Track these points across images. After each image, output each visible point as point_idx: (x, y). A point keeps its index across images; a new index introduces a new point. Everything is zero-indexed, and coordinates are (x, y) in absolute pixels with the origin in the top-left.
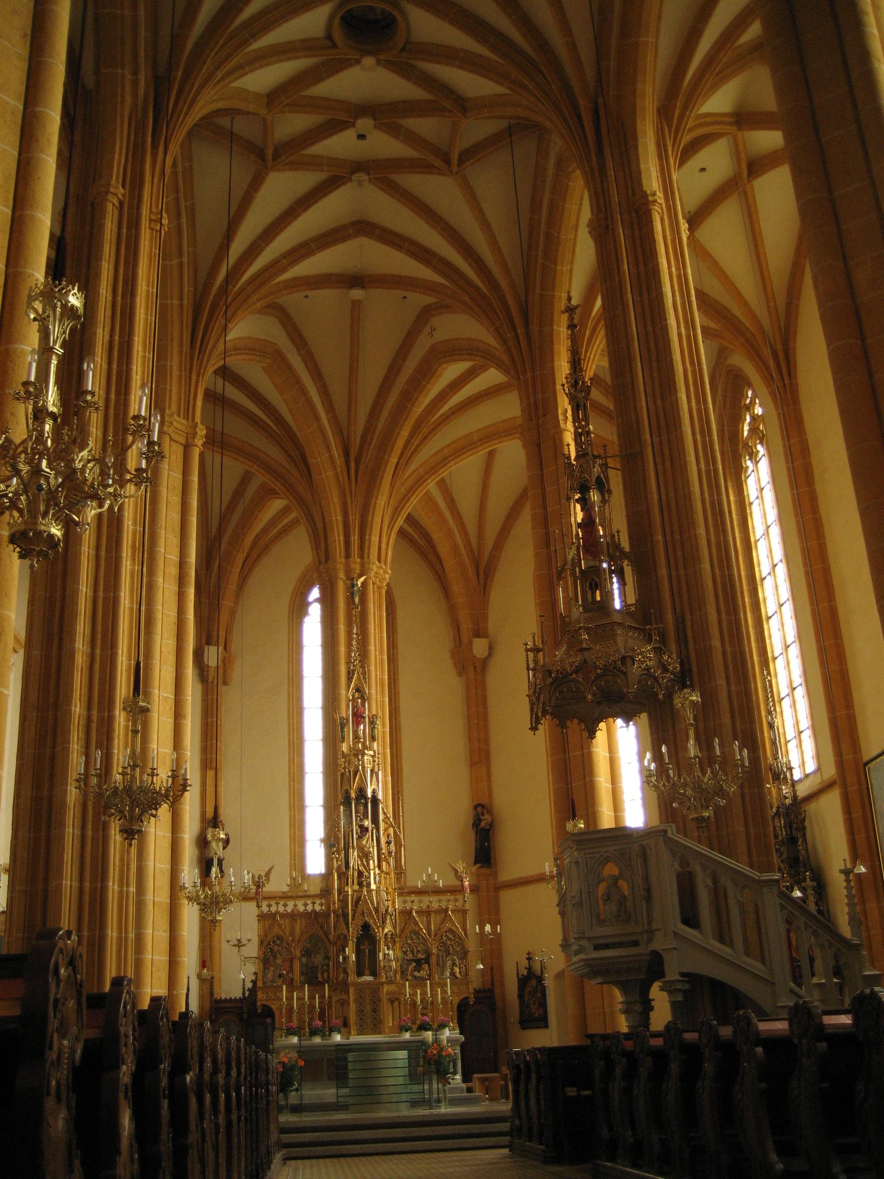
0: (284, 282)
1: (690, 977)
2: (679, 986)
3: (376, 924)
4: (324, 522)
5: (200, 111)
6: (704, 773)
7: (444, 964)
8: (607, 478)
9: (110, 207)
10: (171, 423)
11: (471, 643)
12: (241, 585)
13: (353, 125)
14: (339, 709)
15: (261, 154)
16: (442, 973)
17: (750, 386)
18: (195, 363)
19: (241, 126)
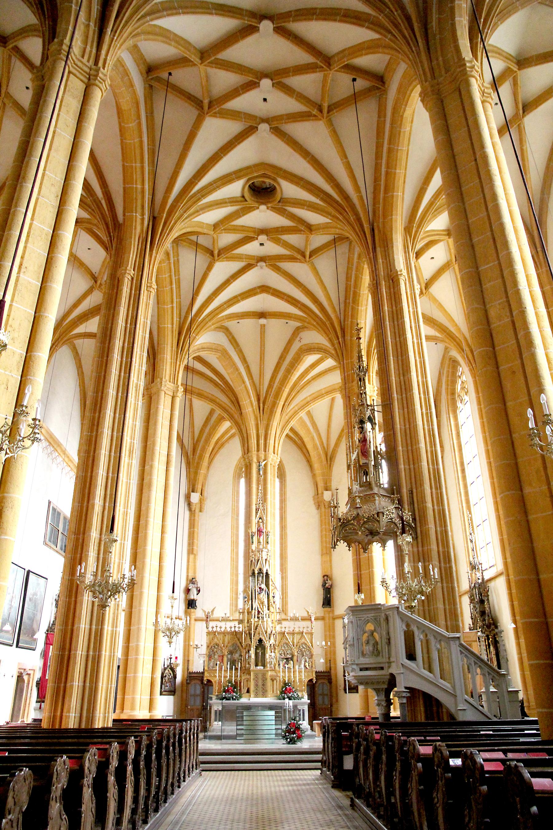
0: (226, 315)
1: (411, 690)
2: (404, 695)
3: (265, 639)
4: (247, 434)
5: (175, 234)
6: (413, 581)
7: (301, 661)
8: (374, 417)
9: (126, 280)
10: (165, 385)
11: (323, 493)
12: (210, 463)
13: (257, 239)
14: (251, 527)
15: (212, 254)
16: (299, 666)
17: (461, 366)
18: (179, 356)
19: (202, 240)
